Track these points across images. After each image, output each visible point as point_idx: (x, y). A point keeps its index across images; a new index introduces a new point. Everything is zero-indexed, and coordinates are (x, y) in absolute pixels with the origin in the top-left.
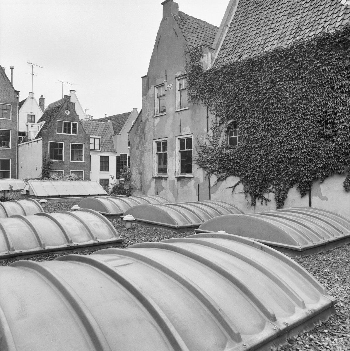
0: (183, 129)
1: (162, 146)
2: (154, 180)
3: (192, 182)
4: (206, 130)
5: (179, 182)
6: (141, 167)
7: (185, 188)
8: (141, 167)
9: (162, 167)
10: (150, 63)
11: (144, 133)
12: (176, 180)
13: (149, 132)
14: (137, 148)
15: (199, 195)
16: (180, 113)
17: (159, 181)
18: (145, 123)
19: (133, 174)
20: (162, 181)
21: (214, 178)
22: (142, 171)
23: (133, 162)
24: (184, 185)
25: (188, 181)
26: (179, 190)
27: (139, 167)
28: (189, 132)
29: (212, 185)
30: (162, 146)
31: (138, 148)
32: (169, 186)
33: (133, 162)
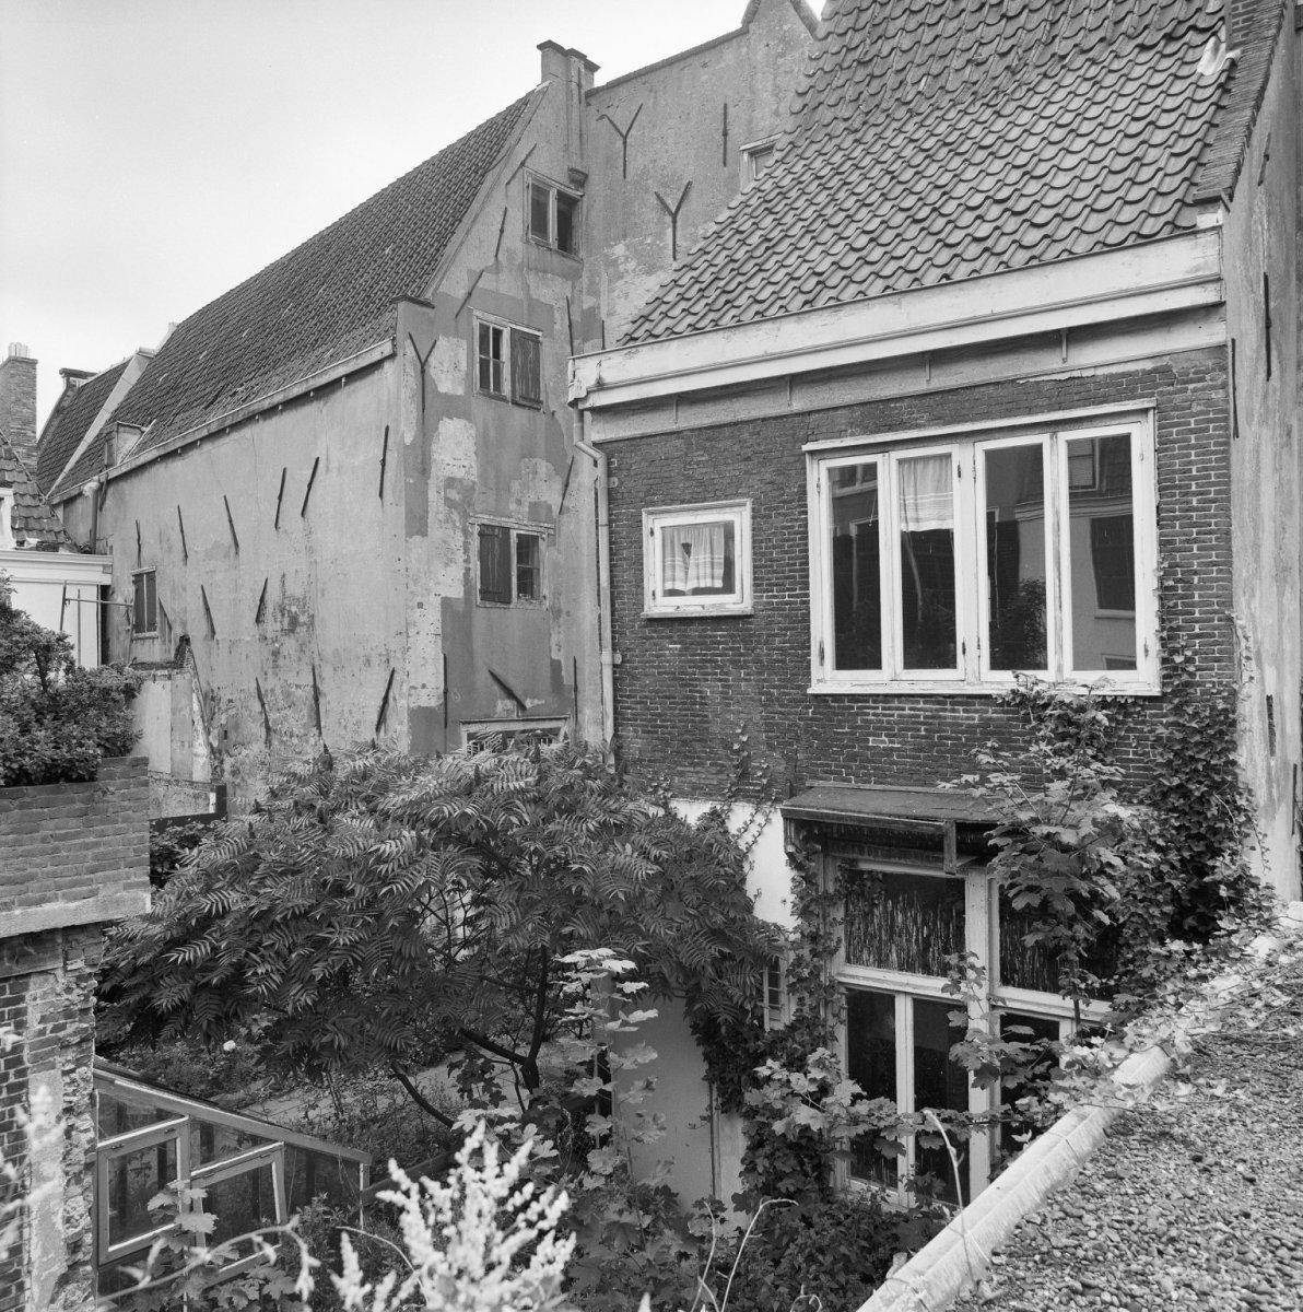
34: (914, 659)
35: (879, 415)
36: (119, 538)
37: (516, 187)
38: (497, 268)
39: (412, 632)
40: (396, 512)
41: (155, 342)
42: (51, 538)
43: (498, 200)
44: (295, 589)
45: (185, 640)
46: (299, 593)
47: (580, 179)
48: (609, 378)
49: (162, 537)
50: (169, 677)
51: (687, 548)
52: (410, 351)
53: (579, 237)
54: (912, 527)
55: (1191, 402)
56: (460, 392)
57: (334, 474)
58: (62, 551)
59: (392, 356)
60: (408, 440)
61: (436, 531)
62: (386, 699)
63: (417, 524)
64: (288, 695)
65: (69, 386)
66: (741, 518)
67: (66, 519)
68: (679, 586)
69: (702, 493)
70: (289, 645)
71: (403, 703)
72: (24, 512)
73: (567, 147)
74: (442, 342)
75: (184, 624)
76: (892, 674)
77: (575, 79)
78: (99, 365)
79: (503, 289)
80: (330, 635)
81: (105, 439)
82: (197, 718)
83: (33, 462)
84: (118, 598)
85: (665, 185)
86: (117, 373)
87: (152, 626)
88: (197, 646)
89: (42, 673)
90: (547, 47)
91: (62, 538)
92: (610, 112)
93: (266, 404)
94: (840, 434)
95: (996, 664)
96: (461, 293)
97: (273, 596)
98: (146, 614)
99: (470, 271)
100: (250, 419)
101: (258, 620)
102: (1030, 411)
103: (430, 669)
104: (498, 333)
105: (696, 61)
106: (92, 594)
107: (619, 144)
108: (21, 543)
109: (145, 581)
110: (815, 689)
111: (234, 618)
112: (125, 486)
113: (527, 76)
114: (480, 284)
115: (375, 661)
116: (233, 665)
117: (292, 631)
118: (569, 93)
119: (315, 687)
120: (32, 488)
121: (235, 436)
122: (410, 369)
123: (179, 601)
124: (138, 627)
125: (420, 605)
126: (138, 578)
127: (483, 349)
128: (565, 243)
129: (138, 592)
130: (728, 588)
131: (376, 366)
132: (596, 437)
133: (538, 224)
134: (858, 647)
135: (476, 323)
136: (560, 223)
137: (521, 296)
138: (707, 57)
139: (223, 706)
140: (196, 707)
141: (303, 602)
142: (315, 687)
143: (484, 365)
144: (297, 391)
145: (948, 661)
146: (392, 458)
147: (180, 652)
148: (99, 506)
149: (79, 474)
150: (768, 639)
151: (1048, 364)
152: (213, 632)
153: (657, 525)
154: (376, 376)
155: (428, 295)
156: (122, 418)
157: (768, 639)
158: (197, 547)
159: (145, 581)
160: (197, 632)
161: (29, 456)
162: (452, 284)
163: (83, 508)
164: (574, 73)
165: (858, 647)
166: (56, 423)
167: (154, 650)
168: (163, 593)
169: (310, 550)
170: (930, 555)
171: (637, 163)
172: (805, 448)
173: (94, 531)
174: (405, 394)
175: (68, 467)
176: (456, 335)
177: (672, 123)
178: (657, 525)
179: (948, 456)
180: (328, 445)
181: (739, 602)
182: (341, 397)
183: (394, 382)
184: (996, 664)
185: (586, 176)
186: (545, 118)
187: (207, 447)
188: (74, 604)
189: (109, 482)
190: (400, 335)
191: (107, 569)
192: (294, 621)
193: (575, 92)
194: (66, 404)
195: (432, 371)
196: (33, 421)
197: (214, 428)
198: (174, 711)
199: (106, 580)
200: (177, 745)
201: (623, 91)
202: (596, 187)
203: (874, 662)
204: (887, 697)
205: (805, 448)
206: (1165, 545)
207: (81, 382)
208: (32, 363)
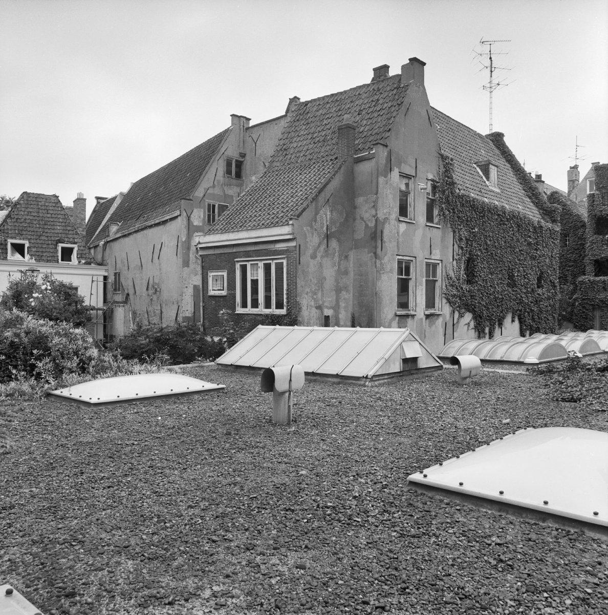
0: (433, 252)
1: (404, 268)
2: (397, 318)
3: (440, 320)
4: (452, 260)
5: (428, 320)
6: (319, 295)
7: (433, 328)
8: (319, 295)
9: (403, 300)
10: (351, 89)
11: (382, 240)
12: (424, 318)
13: (390, 241)
14: (314, 257)
15: (445, 335)
16: (431, 229)
17: (403, 320)
18: (384, 223)
19: (304, 308)
20: (407, 320)
21: (457, 315)
22: (321, 302)
23: (303, 283)
24: (432, 325)
25: (437, 319)
26: (427, 331)
27: (315, 294)
28: (438, 257)
29: (455, 322)
30: (404, 268)
31: (316, 257)
32: (417, 326)
33: (303, 283)
34: (277, 308)
35: (247, 254)
36: (110, 261)
37: (221, 161)
38: (214, 186)
39: (184, 295)
40: (180, 261)
41: (125, 189)
42: (89, 260)
43: (215, 166)
44: (156, 281)
45: (128, 295)
46: (157, 282)
47: (243, 155)
48: (201, 241)
49: (122, 262)
50: (124, 306)
51: (216, 280)
52: (185, 214)
53: (243, 174)
54: (253, 278)
55: (294, 256)
56: (201, 224)
57: (166, 248)
58: (92, 265)
59: (180, 215)
60: (184, 240)
61: (192, 266)
62: (177, 314)
63: (186, 263)
64: (154, 312)
65: (98, 203)
66: (225, 274)
67: (95, 252)
68: (215, 288)
69: (219, 268)
70: (155, 297)
71: (181, 315)
72: (80, 252)
73: (239, 146)
74: (195, 210)
75: (128, 289)
76: (249, 310)
77: (242, 124)
78: (109, 196)
79: (216, 192)
80: (165, 295)
81: (106, 227)
82: (131, 319)
83: (84, 233)
84: (110, 280)
85: (265, 159)
86: (114, 199)
87: (119, 290)
88: (131, 297)
89: (76, 306)
90: (233, 116)
91: (92, 260)
92: (252, 135)
93: (150, 224)
94: (241, 257)
95: (283, 308)
96: (202, 195)
97: (151, 282)
98: (118, 286)
99: (205, 189)
100: (146, 228)
101: (147, 290)
102: (270, 256)
103: (189, 305)
104: (214, 206)
105: (274, 123)
106: (101, 279)
107: (254, 145)
108: (80, 262)
109: (117, 275)
110: (237, 312)
111: (141, 289)
112: (112, 244)
113: (227, 123)
114: (208, 192)
115: (175, 303)
116: (140, 303)
117: (156, 293)
118: (240, 129)
119: (161, 310)
120: (83, 244)
121: (142, 232)
122: (185, 219)
123: (126, 282)
124: (115, 290)
125: (187, 287)
126: (115, 274)
127: (209, 211)
128: (239, 175)
129: (115, 278)
130: (223, 290)
131: (177, 217)
132: (200, 254)
133: (229, 172)
134: (244, 305)
135: (207, 204)
136: (236, 169)
137: (222, 194)
138: (276, 122)
139: (138, 315)
140: (131, 316)
141: (158, 284)
142: (161, 310)
143: (209, 216)
144: (157, 221)
145: (257, 307)
146: (179, 244)
147: (127, 298)
148: (104, 249)
149: (99, 238)
150: (228, 302)
151: (271, 247)
152: (135, 292)
153: (211, 274)
154: (176, 220)
155: (191, 197)
156: (112, 220)
157: (228, 302)
158: (132, 266)
159: (117, 275)
160: (131, 292)
161: (83, 231)
162: (199, 193)
163: (100, 249)
164: (242, 123)
165: (244, 305)
166: (93, 215)
167: (119, 298)
168: (122, 280)
169: (160, 269)
170: (255, 283)
171: (258, 152)
172: (236, 260)
173: (103, 257)
174: (183, 226)
175: (96, 234)
176: (200, 207)
177: (268, 140)
178: (211, 274)
179: (257, 264)
180: (164, 239)
181: (224, 293)
182: (168, 224)
183: (180, 223)
184: (283, 308)
185: (245, 154)
186: (232, 139)
187: (135, 235)
188: (95, 283)
189: (108, 242)
190: (182, 209)
191: (107, 270)
192: (156, 290)
193: (242, 129)
194: (97, 209)
195: (192, 219)
196: (85, 219)
197: (136, 229)
198: (125, 317)
199: (106, 274)
200: (125, 328)
201: (256, 128)
202: (247, 157)
203: (246, 307)
204: (248, 314)
205: (236, 260)
206: (287, 284)
207: (102, 201)
208: (85, 200)
